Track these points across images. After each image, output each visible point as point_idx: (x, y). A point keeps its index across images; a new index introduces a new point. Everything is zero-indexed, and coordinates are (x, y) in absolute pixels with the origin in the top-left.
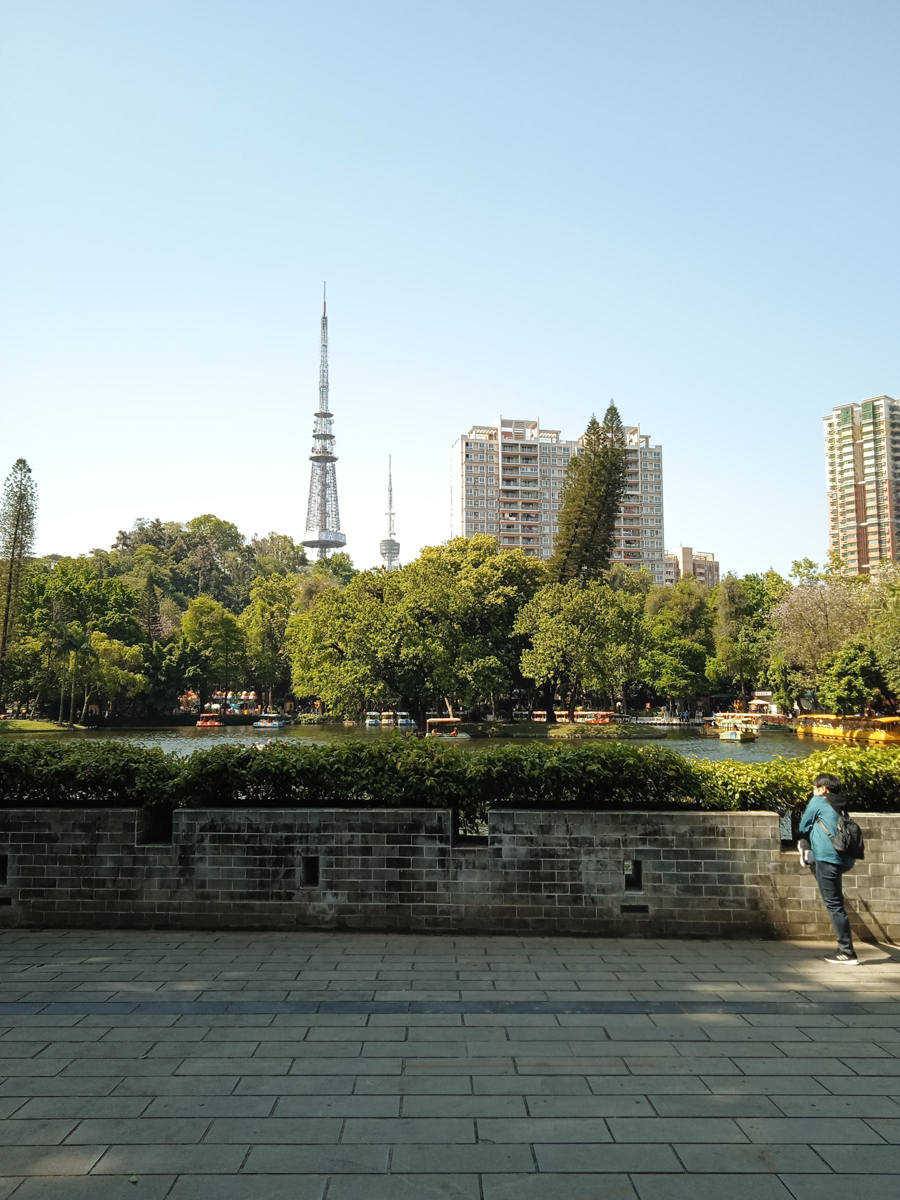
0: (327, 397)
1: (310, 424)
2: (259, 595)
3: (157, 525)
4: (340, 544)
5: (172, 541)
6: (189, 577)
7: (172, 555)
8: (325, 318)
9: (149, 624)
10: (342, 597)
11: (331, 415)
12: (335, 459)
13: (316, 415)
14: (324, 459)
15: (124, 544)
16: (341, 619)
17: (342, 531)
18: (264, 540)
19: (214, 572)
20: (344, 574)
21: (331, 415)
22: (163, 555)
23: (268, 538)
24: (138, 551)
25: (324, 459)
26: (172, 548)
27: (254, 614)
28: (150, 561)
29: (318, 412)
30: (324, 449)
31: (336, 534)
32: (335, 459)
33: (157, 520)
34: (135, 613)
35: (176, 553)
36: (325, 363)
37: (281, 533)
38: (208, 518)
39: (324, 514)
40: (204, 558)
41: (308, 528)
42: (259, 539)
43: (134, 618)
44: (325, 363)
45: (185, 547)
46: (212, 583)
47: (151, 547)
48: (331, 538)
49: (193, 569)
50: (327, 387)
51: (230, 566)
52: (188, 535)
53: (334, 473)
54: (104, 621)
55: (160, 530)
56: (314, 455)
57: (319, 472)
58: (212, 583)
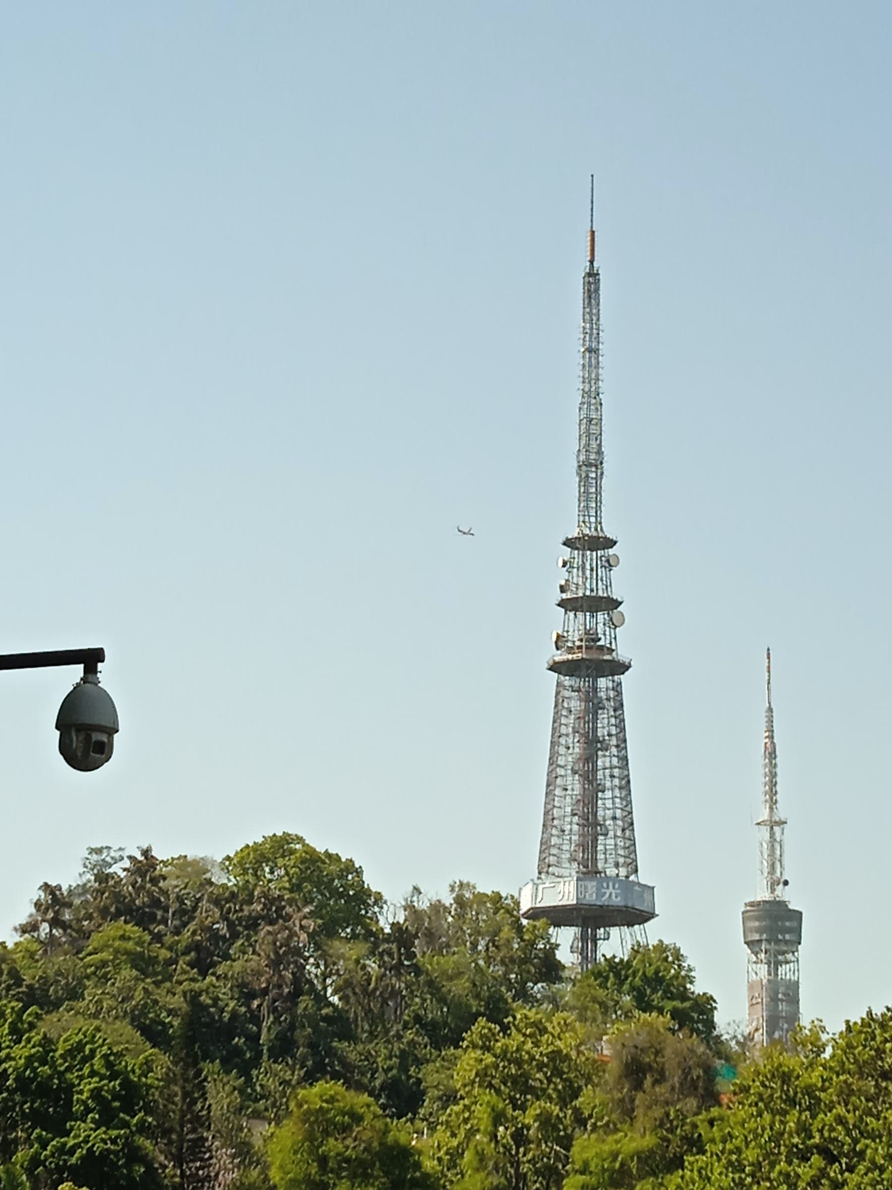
0: (598, 493)
1: (551, 571)
2: (483, 1077)
3: (145, 866)
4: (636, 916)
5: (186, 914)
6: (234, 1014)
7: (186, 952)
8: (592, 276)
9: (179, 1161)
10: (809, 1091)
11: (612, 543)
12: (623, 668)
13: (568, 543)
14: (590, 668)
15: (55, 922)
16: (815, 1159)
17: (644, 877)
18: (438, 908)
19: (305, 1003)
20: (669, 1005)
21: (612, 543)
22: (165, 954)
23: (448, 900)
24: (95, 941)
25: (590, 668)
26: (186, 934)
27: (471, 1133)
28: (128, 972)
29: (574, 533)
30: (591, 638)
31: (627, 886)
32: (623, 668)
33: (146, 853)
34: (142, 1128)
35: (196, 947)
36: (592, 397)
37: (485, 887)
38: (281, 845)
39: (591, 826)
40: (276, 963)
41: (544, 868)
42: (423, 904)
43: (147, 1144)
44: (592, 397)
45: (222, 928)
46: (303, 1034)
47: (132, 929)
48: (613, 897)
49: (246, 994)
50: (598, 464)
51: (348, 984)
52: (233, 895)
53: (619, 707)
54: (62, 1150)
55: (154, 881)
56: (561, 656)
57: (576, 704)
58: (303, 1034)
